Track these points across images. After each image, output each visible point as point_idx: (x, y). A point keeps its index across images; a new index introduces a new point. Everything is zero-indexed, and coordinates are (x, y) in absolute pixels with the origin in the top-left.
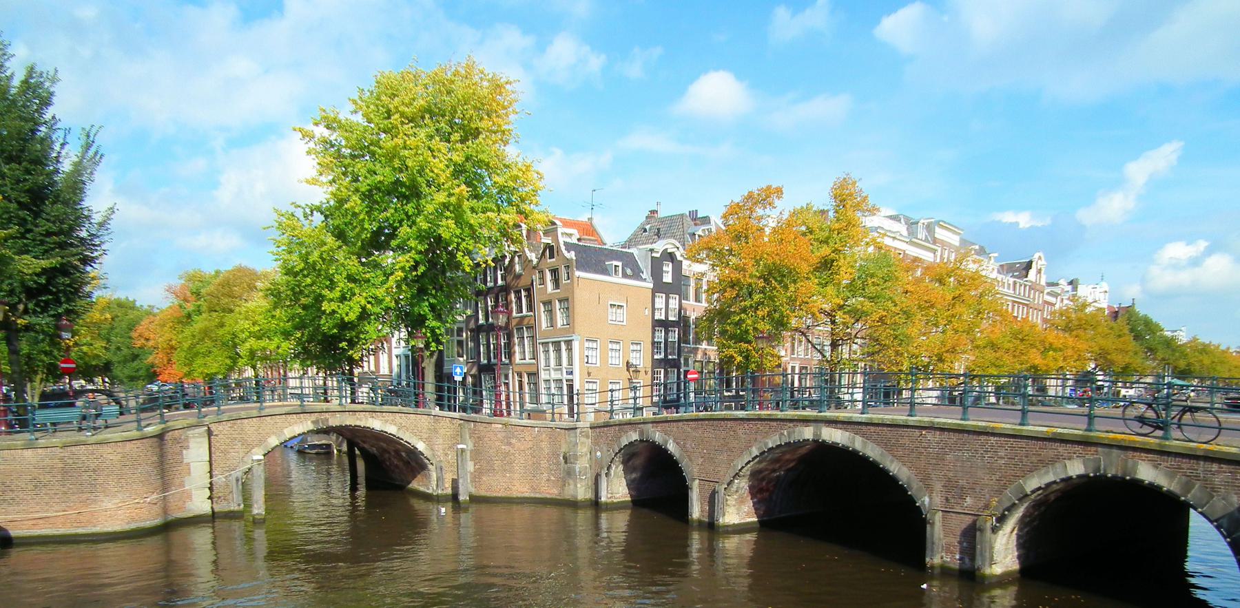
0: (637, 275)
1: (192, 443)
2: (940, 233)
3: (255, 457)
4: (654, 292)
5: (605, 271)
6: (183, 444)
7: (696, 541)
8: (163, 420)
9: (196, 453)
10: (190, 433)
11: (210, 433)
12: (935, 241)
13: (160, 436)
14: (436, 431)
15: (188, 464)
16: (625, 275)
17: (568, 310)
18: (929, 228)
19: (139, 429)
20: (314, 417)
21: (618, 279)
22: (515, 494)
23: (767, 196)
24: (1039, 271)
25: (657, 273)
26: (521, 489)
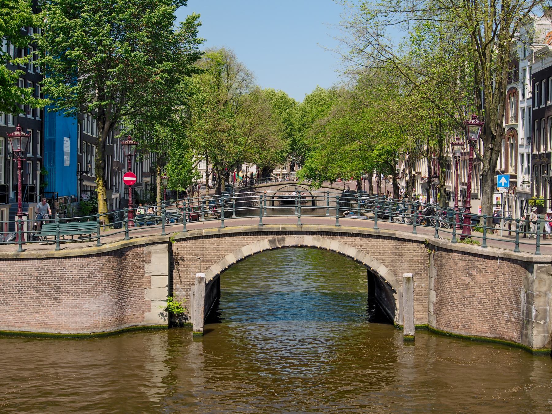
1: (154, 258)
13: (119, 253)
14: (400, 255)
15: (149, 278)
20: (270, 237)
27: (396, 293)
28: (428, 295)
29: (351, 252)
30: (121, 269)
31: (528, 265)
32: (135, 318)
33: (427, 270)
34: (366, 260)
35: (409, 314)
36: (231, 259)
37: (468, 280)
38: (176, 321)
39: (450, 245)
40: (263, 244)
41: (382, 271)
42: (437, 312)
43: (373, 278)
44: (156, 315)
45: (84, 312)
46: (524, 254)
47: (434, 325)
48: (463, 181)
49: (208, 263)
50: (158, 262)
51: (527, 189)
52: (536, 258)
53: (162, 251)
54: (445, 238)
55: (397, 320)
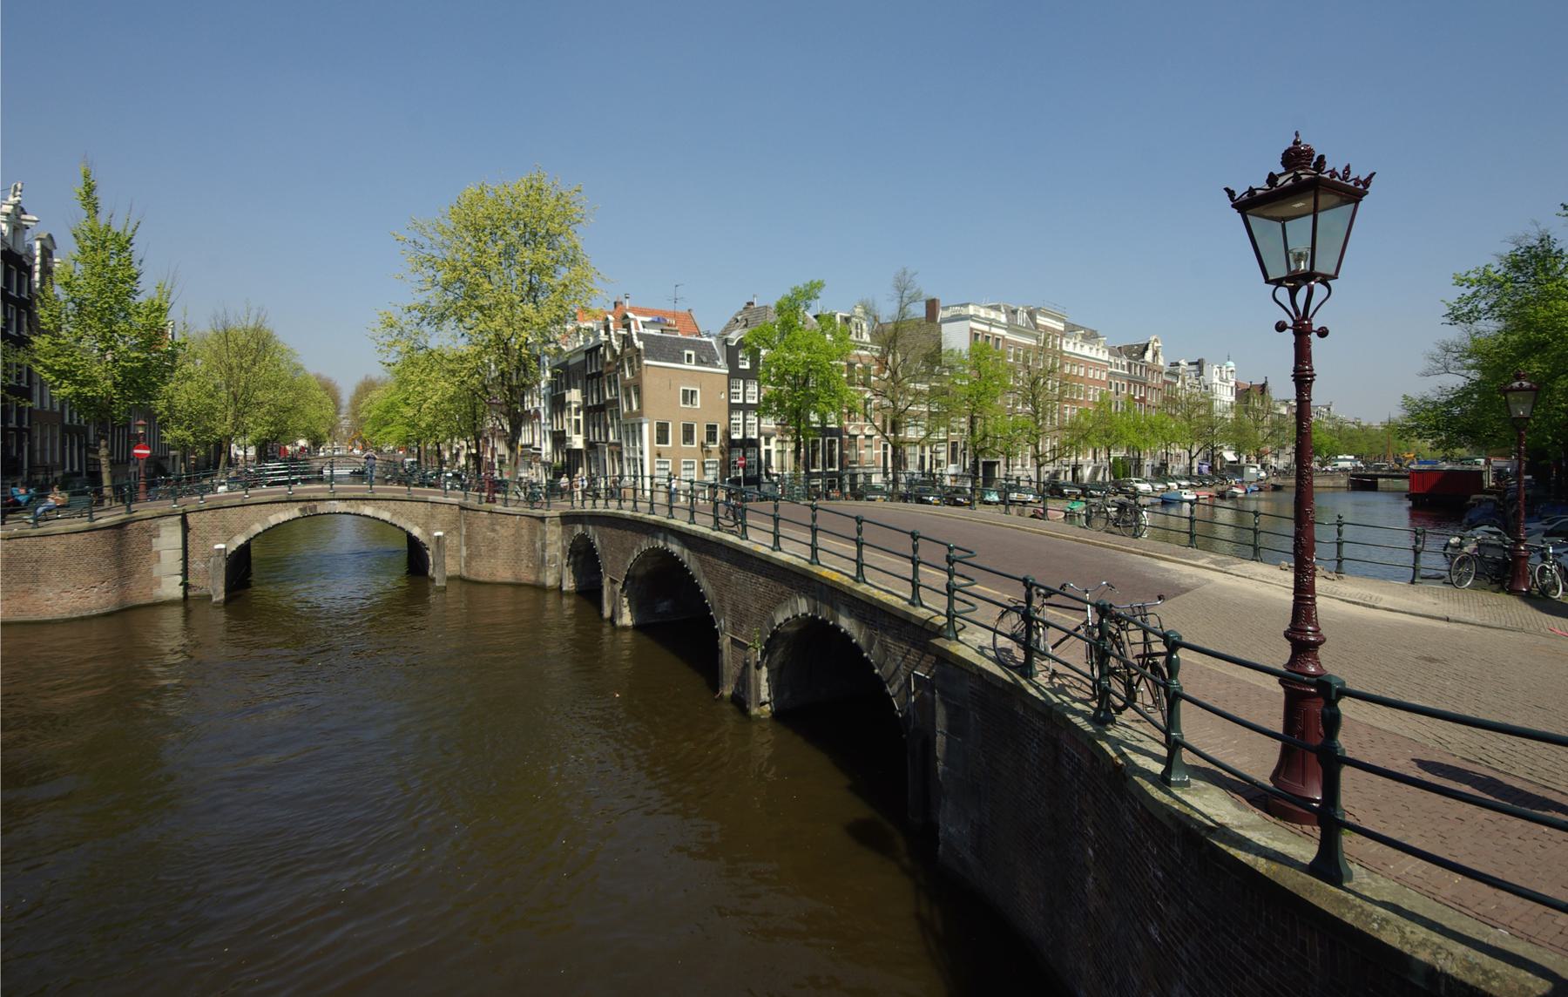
0: (712, 362)
1: (164, 532)
2: (1041, 320)
3: (1341, 465)
4: (731, 376)
5: (679, 359)
6: (153, 534)
7: (607, 630)
8: (129, 511)
9: (168, 540)
10: (162, 522)
11: (184, 522)
12: (1037, 326)
13: (120, 526)
14: (433, 516)
15: (158, 553)
16: (699, 362)
17: (639, 393)
18: (1032, 315)
19: (91, 520)
20: (301, 505)
21: (692, 366)
22: (499, 580)
23: (809, 293)
24: (1155, 354)
25: (732, 360)
26: (505, 575)
27: (809, 293)
28: (459, 551)
29: (386, 516)
30: (121, 545)
31: (542, 519)
32: (138, 596)
33: (458, 529)
34: (401, 523)
35: (447, 565)
36: (258, 528)
37: (492, 535)
38: (188, 602)
39: (476, 505)
40: (293, 512)
41: (416, 532)
42: (468, 564)
43: (412, 540)
44: (171, 588)
45: (70, 594)
46: (537, 512)
47: (465, 574)
48: (67, 421)
49: (230, 535)
50: (168, 540)
51: (549, 459)
52: (547, 514)
53: (173, 524)
54: (472, 500)
55: (430, 572)
